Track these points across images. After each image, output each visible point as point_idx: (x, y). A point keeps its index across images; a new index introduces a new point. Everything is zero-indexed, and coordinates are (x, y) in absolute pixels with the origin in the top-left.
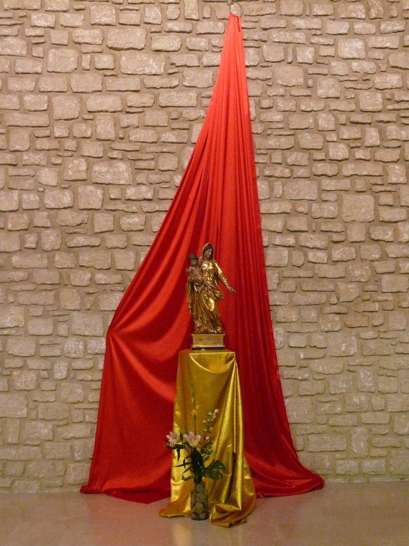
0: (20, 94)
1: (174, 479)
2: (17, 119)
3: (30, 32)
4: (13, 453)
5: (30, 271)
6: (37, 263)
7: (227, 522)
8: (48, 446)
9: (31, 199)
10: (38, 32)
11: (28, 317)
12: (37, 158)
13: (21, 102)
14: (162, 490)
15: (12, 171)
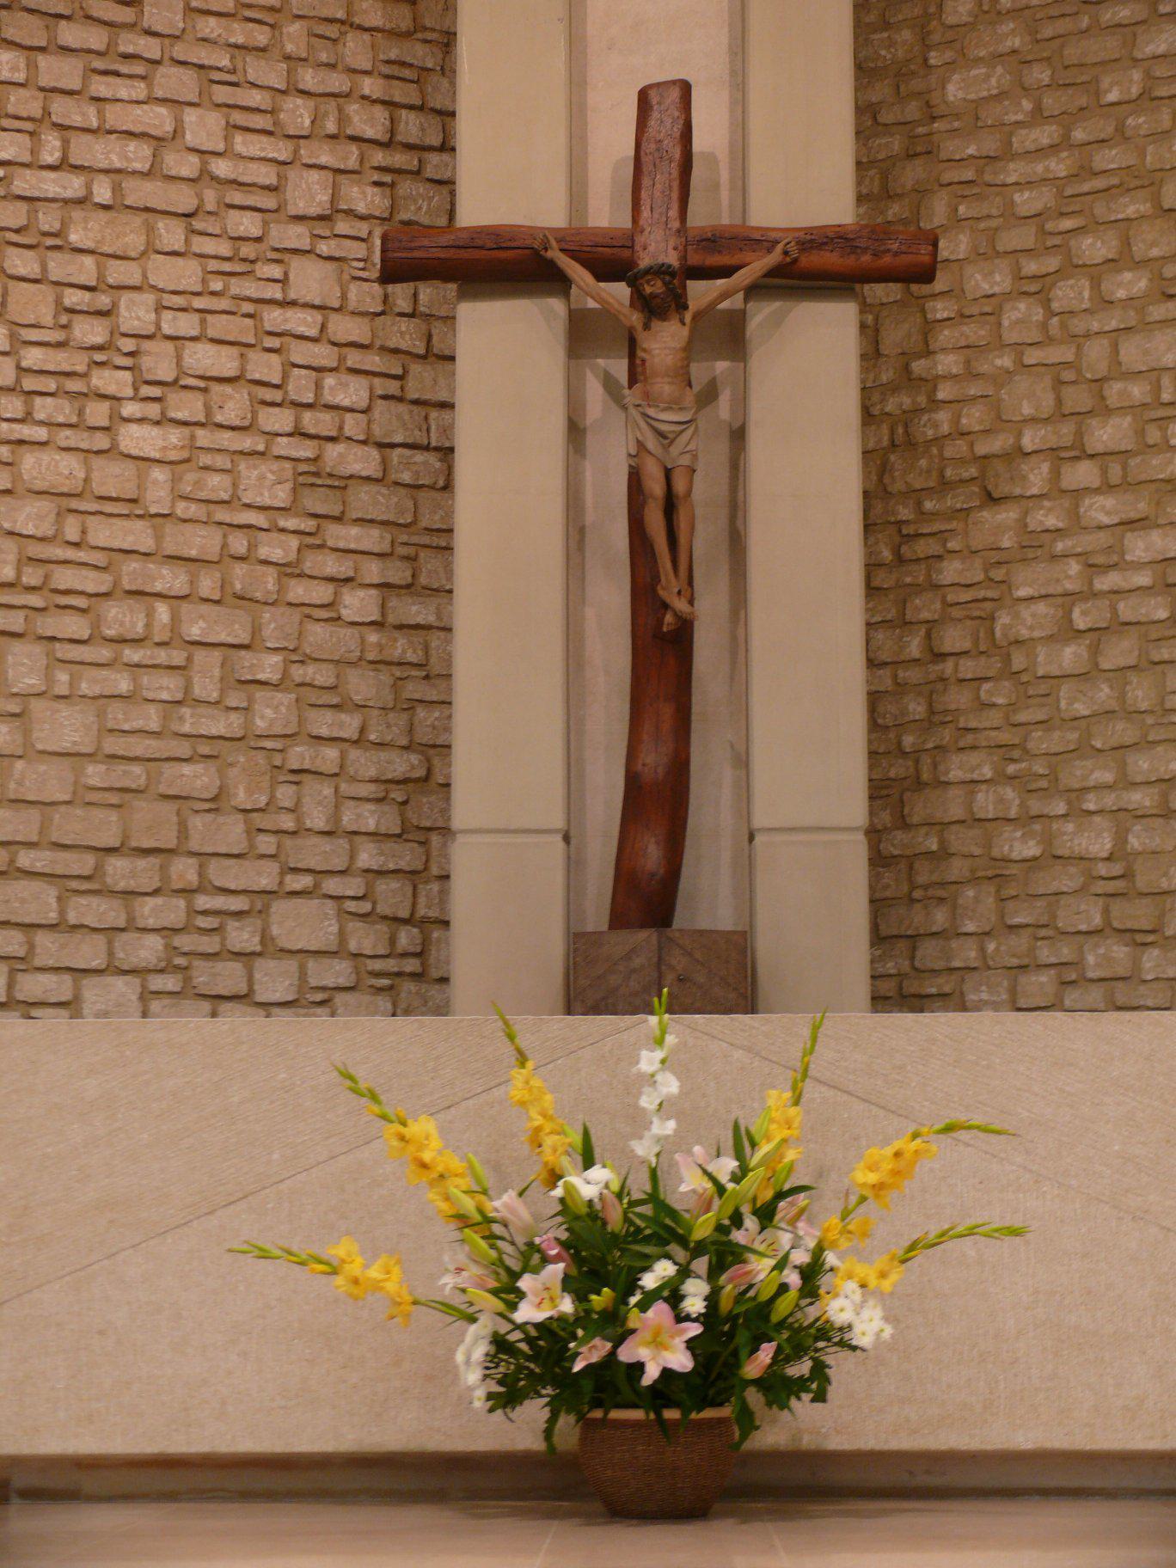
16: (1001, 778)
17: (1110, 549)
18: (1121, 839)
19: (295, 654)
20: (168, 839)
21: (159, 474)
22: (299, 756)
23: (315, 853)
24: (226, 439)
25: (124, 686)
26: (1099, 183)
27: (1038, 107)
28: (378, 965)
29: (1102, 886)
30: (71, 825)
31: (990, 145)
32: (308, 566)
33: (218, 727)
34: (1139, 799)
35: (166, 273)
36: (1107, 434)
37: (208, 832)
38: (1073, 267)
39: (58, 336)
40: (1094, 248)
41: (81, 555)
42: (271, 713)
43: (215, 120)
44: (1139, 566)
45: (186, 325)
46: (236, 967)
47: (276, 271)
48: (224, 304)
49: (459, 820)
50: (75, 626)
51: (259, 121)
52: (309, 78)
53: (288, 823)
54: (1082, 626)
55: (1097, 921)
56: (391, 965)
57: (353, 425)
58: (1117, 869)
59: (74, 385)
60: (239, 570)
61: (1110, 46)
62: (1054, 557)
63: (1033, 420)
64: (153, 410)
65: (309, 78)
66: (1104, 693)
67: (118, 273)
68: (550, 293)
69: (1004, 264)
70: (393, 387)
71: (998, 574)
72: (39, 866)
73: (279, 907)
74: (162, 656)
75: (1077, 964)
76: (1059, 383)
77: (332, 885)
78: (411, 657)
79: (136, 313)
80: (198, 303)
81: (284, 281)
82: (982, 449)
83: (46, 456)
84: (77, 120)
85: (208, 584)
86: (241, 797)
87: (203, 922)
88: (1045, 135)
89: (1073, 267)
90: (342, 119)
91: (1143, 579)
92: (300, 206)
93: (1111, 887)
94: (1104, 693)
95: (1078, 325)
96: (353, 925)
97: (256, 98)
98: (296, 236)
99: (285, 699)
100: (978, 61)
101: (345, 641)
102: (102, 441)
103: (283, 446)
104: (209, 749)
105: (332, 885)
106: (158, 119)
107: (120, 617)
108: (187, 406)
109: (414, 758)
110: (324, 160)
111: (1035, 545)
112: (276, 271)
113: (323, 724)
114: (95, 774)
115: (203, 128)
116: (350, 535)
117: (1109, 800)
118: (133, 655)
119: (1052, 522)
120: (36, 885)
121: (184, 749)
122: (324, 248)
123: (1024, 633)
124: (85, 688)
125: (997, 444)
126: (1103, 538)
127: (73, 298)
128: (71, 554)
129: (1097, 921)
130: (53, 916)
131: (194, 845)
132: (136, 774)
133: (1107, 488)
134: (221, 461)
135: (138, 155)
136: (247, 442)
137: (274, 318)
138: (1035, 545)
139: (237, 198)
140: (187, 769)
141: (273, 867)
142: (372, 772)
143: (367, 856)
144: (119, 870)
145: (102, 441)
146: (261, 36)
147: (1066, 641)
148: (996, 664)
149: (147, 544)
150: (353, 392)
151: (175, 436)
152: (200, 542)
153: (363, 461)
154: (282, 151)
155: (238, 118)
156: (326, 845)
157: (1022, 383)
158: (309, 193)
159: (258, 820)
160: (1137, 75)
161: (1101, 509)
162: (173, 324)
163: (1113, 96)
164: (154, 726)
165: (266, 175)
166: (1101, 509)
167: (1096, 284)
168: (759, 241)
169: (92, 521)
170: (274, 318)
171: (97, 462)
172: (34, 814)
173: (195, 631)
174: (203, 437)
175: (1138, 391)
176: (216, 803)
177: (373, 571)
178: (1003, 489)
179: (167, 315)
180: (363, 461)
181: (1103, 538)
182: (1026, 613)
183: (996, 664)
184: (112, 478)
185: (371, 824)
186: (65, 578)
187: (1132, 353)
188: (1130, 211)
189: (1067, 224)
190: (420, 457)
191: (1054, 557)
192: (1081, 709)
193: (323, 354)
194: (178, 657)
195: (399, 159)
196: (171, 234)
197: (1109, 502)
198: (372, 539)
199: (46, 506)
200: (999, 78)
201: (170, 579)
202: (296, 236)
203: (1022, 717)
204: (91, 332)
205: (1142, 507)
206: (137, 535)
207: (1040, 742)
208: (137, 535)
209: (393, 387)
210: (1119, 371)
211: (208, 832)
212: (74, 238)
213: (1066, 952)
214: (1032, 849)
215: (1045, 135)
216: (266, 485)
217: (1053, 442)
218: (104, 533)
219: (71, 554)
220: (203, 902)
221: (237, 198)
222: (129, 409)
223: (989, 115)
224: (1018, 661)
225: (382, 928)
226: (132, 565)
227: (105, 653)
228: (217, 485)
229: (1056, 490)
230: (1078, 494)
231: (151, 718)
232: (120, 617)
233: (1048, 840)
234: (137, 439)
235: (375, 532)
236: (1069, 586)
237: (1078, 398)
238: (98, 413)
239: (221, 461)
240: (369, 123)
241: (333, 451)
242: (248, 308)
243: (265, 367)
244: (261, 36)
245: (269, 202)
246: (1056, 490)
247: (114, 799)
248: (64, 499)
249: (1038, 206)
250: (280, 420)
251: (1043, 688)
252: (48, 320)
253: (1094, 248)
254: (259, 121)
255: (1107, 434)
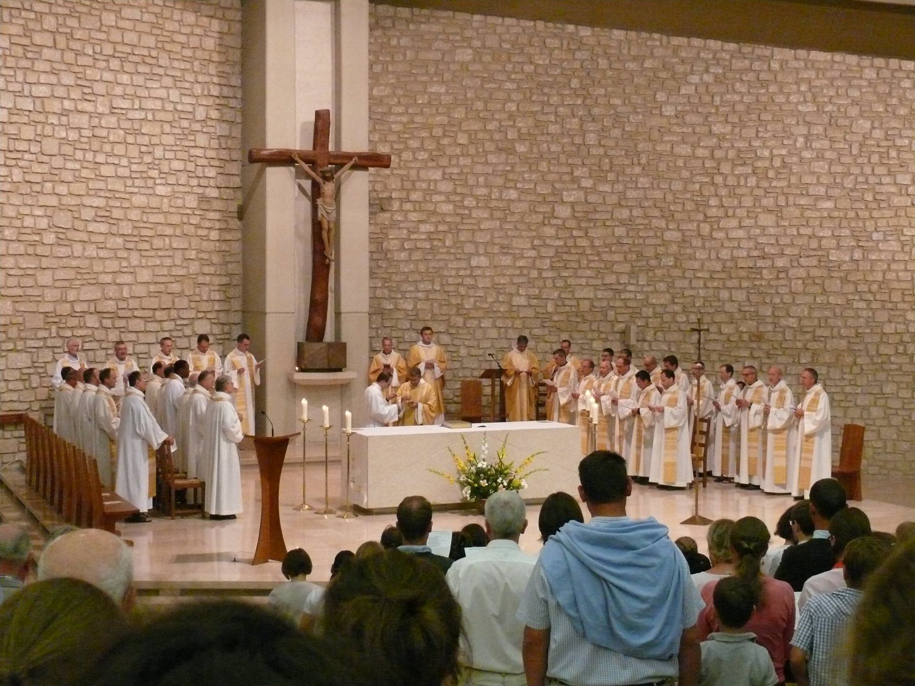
0: (897, 272)
1: (866, 458)
2: (895, 285)
3: (903, 238)
4: (889, 457)
5: (900, 365)
6: (904, 361)
7: (621, 448)
8: (907, 454)
9: (901, 328)
10: (907, 238)
11: (899, 388)
12: (904, 306)
13: (897, 276)
14: (402, 400)
15: (892, 313)
16: (383, 287)
17: (414, 228)
18: (415, 306)
19: (200, 251)
20: (170, 305)
21: (165, 200)
22: (201, 279)
23: (205, 307)
24: (182, 189)
25: (158, 263)
26: (415, 126)
27: (399, 102)
28: (219, 337)
29: (410, 318)
30: (147, 303)
31: (385, 109)
32: (202, 225)
33: (181, 273)
34: (420, 295)
35: (169, 140)
36: (415, 196)
37: (182, 303)
38: (407, 148)
39: (139, 161)
40: (414, 144)
41: (148, 225)
42: (194, 268)
43: (177, 92)
44: (423, 233)
45: (170, 155)
46: (186, 340)
47: (192, 138)
48: (180, 148)
49: (268, 310)
50: (146, 246)
51: (188, 92)
52: (201, 78)
53: (198, 299)
54: (407, 247)
55: (408, 326)
56: (223, 337)
57: (212, 183)
58: (415, 313)
59: (144, 175)
60: (185, 227)
61: (419, 88)
62: (399, 228)
63: (394, 189)
64: (163, 181)
65: (201, 78)
66: (412, 266)
67: (155, 140)
68: (290, 165)
69: (388, 145)
70: (221, 170)
71: (385, 231)
72: (140, 315)
73: (197, 322)
74: (167, 253)
75: (403, 337)
76: (402, 180)
77: (209, 316)
78: (227, 249)
79: (159, 152)
80: (174, 148)
81: (194, 141)
82: (380, 196)
83: (138, 197)
84: (143, 95)
85: (178, 232)
86: (187, 293)
87: (178, 328)
88: (400, 109)
89: (407, 148)
90: (209, 90)
91: (424, 237)
92: (199, 118)
93: (413, 318)
94: (412, 266)
95: (409, 165)
96: (214, 326)
97: (187, 85)
98: (197, 127)
99: (197, 263)
100: (382, 85)
101: (210, 246)
102: (151, 191)
103: (196, 190)
104: (179, 279)
105: (209, 316)
106: (162, 93)
107: (158, 243)
108: (172, 180)
109: (228, 278)
110: (204, 103)
111: (394, 224)
112: (192, 138)
113: (206, 270)
114: (152, 288)
115: (174, 95)
116: (212, 215)
117: (413, 295)
118: (160, 253)
119: (399, 218)
120: (138, 320)
121: (172, 279)
122: (204, 130)
123: (391, 248)
124: (149, 264)
125: (385, 195)
126: (413, 224)
127: (144, 149)
128: (144, 225)
129: (408, 326)
130: (143, 329)
131: (176, 307)
132: (162, 288)
133: (415, 211)
134: (181, 196)
135: (158, 105)
136: (187, 189)
137: (193, 152)
138: (394, 224)
139: (183, 116)
140: (174, 285)
141: (194, 311)
142: (217, 283)
143: (217, 307)
144: (159, 315)
145: (151, 191)
146: (188, 66)
147: (402, 251)
148: (383, 255)
149: (163, 221)
150: (211, 173)
151: (169, 189)
152: (175, 219)
153: (214, 193)
154: (193, 101)
155: (183, 91)
156: (206, 304)
157: (392, 179)
158: (201, 113)
159: (192, 299)
160: (426, 97)
161: (413, 217)
162: (170, 155)
163: (420, 102)
164: (166, 273)
165: (190, 109)
166: (413, 217)
167: (414, 153)
168: (349, 157)
169: (150, 215)
170: (193, 152)
171: (151, 198)
172: (138, 300)
173: (175, 245)
174: (177, 188)
175: (424, 185)
176: (181, 294)
177: (217, 225)
178: (386, 207)
179: (167, 153)
180: (214, 193)
181: (413, 224)
182: (392, 242)
183: (383, 255)
184: (154, 202)
185: (218, 298)
186: (144, 232)
187: (422, 174)
188: (424, 135)
189: (407, 136)
190: (228, 191)
191: (399, 228)
192: (406, 270)
193: (203, 162)
194: (171, 253)
195: (223, 102)
196: (167, 128)
197: (415, 214)
198: (216, 216)
199: (138, 212)
200: (388, 91)
201: (169, 231)
202: (197, 127)
203: (390, 271)
204: (148, 159)
205: (424, 217)
206: (160, 218)
207: (395, 278)
208: (160, 218)
209: (221, 170)
210: (419, 179)
211: (182, 303)
212: (143, 131)
213: (400, 334)
214: (391, 307)
215: (400, 109)
216: (192, 202)
217: (401, 196)
218: (153, 219)
219: (144, 225)
220: (179, 322)
221: (183, 116)
222: (158, 181)
223: (386, 100)
224: (389, 256)
225: (221, 326)
226: (160, 227)
227: (153, 253)
228: (179, 202)
229: (401, 210)
230: (407, 212)
231: (165, 271)
232: (158, 243)
233: (396, 304)
234: (161, 190)
235: (218, 214)
236: (403, 236)
237: (408, 185)
238: (150, 183)
239: (181, 196)
240: (215, 91)
241: (208, 190)
242: (186, 149)
243: (190, 166)
244: (188, 66)
245: (191, 117)
246: (401, 210)
247: (156, 294)
248: (143, 209)
249: (398, 129)
250: (194, 182)
251: (395, 263)
252: (137, 156)
253: (414, 144)
254: (188, 92)
255: (415, 196)
